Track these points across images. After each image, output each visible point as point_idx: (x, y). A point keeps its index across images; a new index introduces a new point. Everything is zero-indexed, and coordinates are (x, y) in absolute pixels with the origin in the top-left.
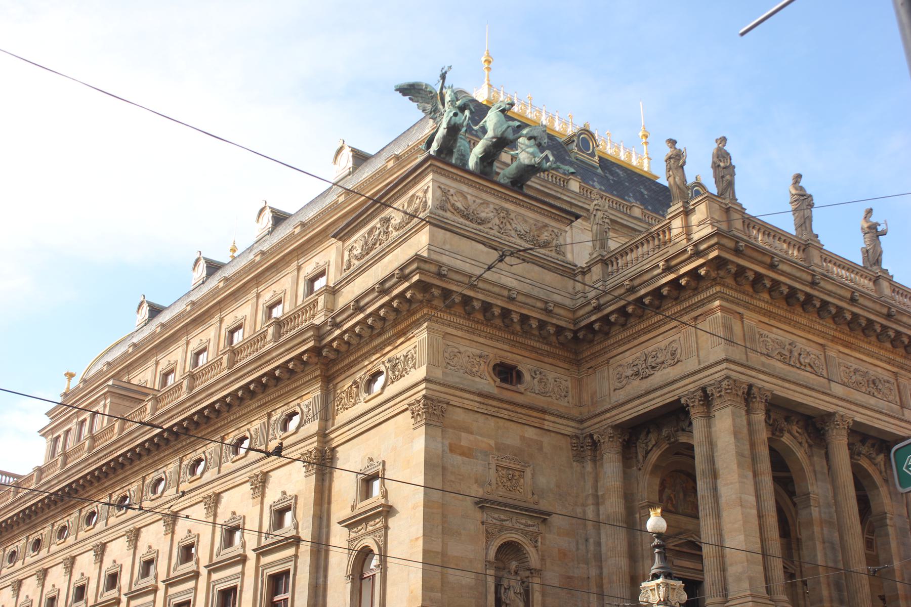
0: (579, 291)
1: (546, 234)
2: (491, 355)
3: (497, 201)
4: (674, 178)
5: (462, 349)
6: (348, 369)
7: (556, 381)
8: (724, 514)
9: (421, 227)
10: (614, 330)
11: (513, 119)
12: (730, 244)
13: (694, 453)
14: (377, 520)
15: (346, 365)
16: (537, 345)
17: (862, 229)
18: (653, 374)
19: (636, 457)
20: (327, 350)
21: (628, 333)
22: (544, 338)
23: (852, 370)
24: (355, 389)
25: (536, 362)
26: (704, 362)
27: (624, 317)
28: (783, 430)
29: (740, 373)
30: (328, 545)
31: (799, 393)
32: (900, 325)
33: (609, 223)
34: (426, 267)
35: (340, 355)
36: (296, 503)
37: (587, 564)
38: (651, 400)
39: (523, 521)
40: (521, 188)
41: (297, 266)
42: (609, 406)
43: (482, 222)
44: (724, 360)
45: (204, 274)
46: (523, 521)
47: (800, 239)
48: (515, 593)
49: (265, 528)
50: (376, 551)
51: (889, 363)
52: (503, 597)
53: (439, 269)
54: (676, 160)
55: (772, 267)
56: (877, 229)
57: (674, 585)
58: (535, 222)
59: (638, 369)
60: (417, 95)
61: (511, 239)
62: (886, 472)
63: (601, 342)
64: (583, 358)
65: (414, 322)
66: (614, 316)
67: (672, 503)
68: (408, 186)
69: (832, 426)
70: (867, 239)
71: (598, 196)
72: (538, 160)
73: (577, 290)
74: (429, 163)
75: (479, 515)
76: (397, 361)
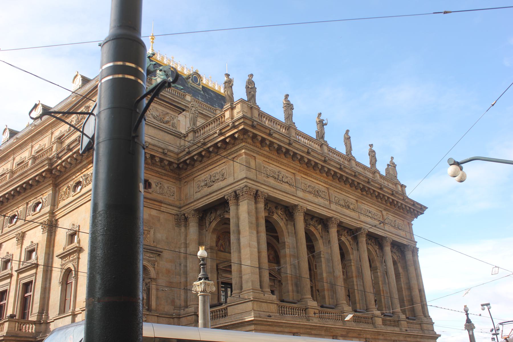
1: (167, 117)
4: (227, 92)
6: (66, 180)
7: (168, 188)
8: (242, 251)
10: (197, 164)
11: (152, 61)
12: (250, 123)
14: (75, 255)
15: (64, 178)
16: (159, 170)
17: (316, 122)
18: (213, 185)
19: (206, 225)
20: (55, 170)
22: (163, 167)
23: (307, 186)
24: (68, 190)
25: (159, 178)
26: (236, 179)
30: (52, 267)
32: (330, 165)
33: (198, 113)
37: (180, 276)
38: (212, 197)
42: (192, 200)
45: (8, 137)
47: (287, 124)
49: (22, 260)
50: (73, 269)
51: (325, 183)
54: (229, 84)
55: (270, 135)
57: (208, 283)
58: (162, 111)
61: (149, 118)
67: (223, 247)
69: (297, 211)
70: (318, 127)
71: (193, 100)
73: (181, 145)
76: (88, 176)
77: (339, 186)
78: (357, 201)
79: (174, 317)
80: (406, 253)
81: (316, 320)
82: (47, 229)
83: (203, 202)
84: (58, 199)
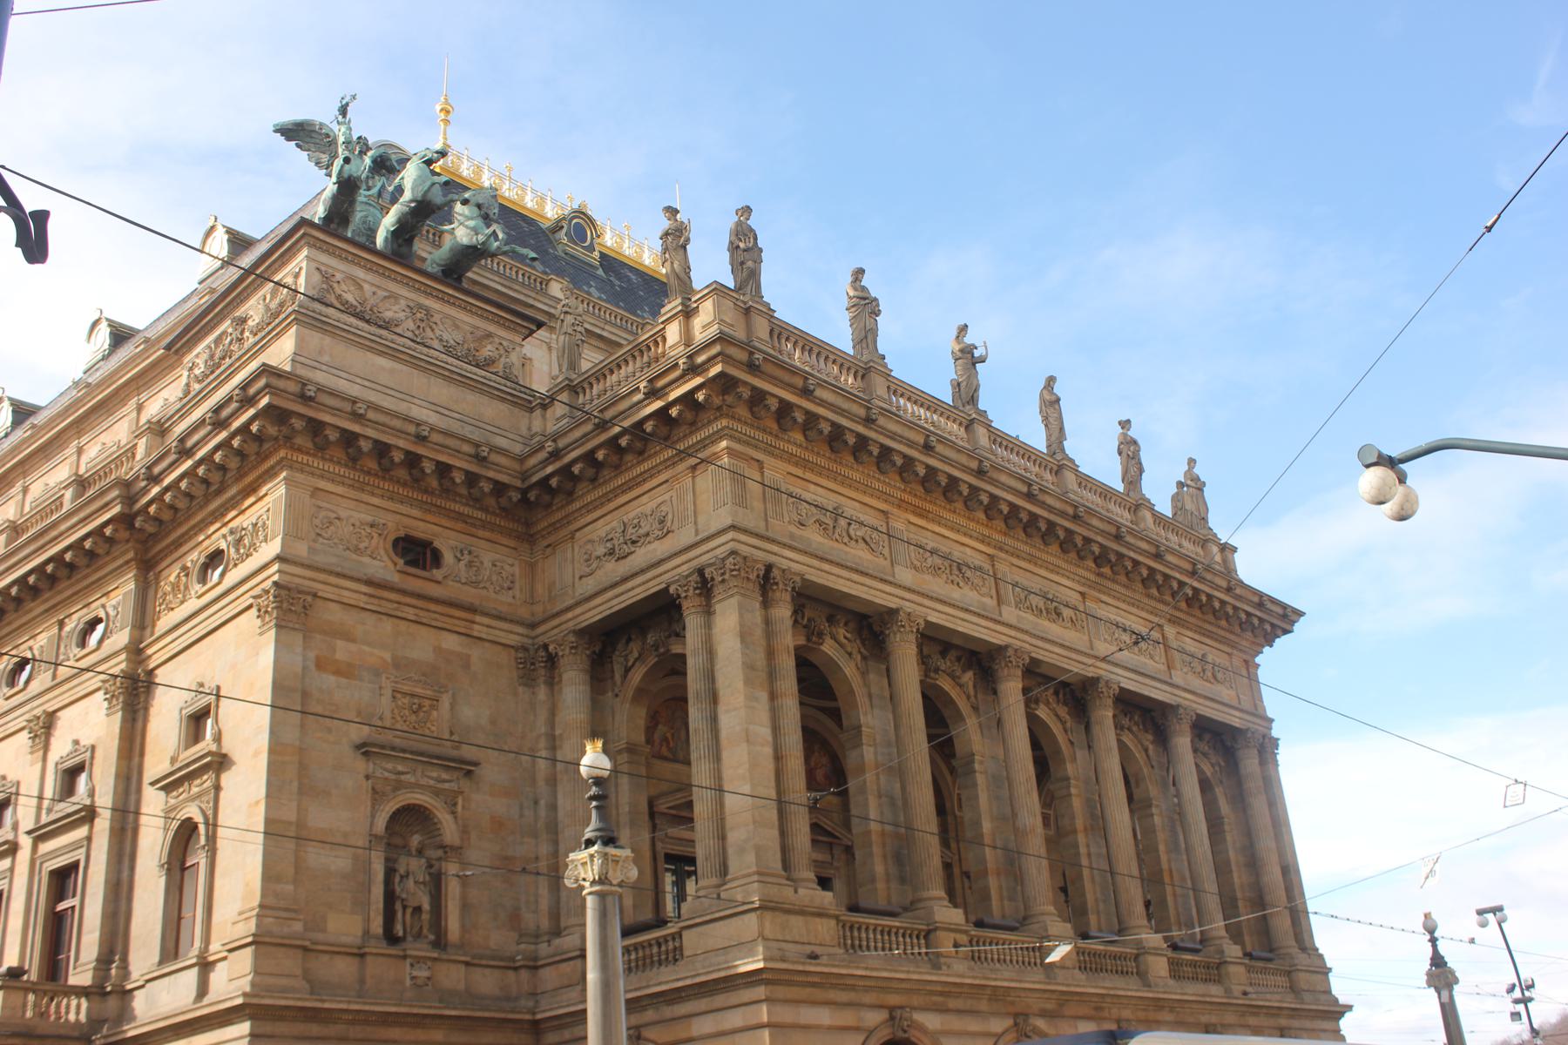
0: (536, 433)
1: (489, 347)
2: (390, 524)
3: (412, 296)
4: (672, 263)
5: (343, 514)
6: (176, 549)
7: (495, 566)
8: (725, 755)
9: (284, 328)
10: (581, 488)
12: (741, 356)
13: (686, 669)
14: (205, 777)
15: (173, 542)
16: (466, 510)
21: (600, 492)
22: (477, 500)
24: (184, 579)
25: (463, 536)
27: (593, 467)
28: (822, 634)
29: (754, 547)
31: (845, 579)
34: (281, 384)
35: (163, 527)
36: (92, 757)
39: (434, 774)
40: (459, 279)
41: (137, 404)
42: (570, 602)
43: (386, 325)
44: (730, 527)
46: (434, 774)
47: (860, 360)
48: (416, 882)
52: (398, 889)
53: (302, 389)
54: (676, 238)
55: (806, 392)
56: (973, 356)
57: (615, 856)
59: (614, 545)
60: (309, 140)
62: (976, 697)
63: (562, 507)
64: (539, 531)
65: (267, 472)
66: (578, 466)
67: (668, 746)
68: (273, 268)
69: (895, 628)
72: (481, 238)
74: (302, 232)
75: (361, 765)
76: (243, 533)
77: (1027, 548)
78: (1083, 594)
79: (518, 964)
80: (1241, 753)
81: (960, 967)
82: (121, 699)
83: (601, 608)
84: (155, 608)
